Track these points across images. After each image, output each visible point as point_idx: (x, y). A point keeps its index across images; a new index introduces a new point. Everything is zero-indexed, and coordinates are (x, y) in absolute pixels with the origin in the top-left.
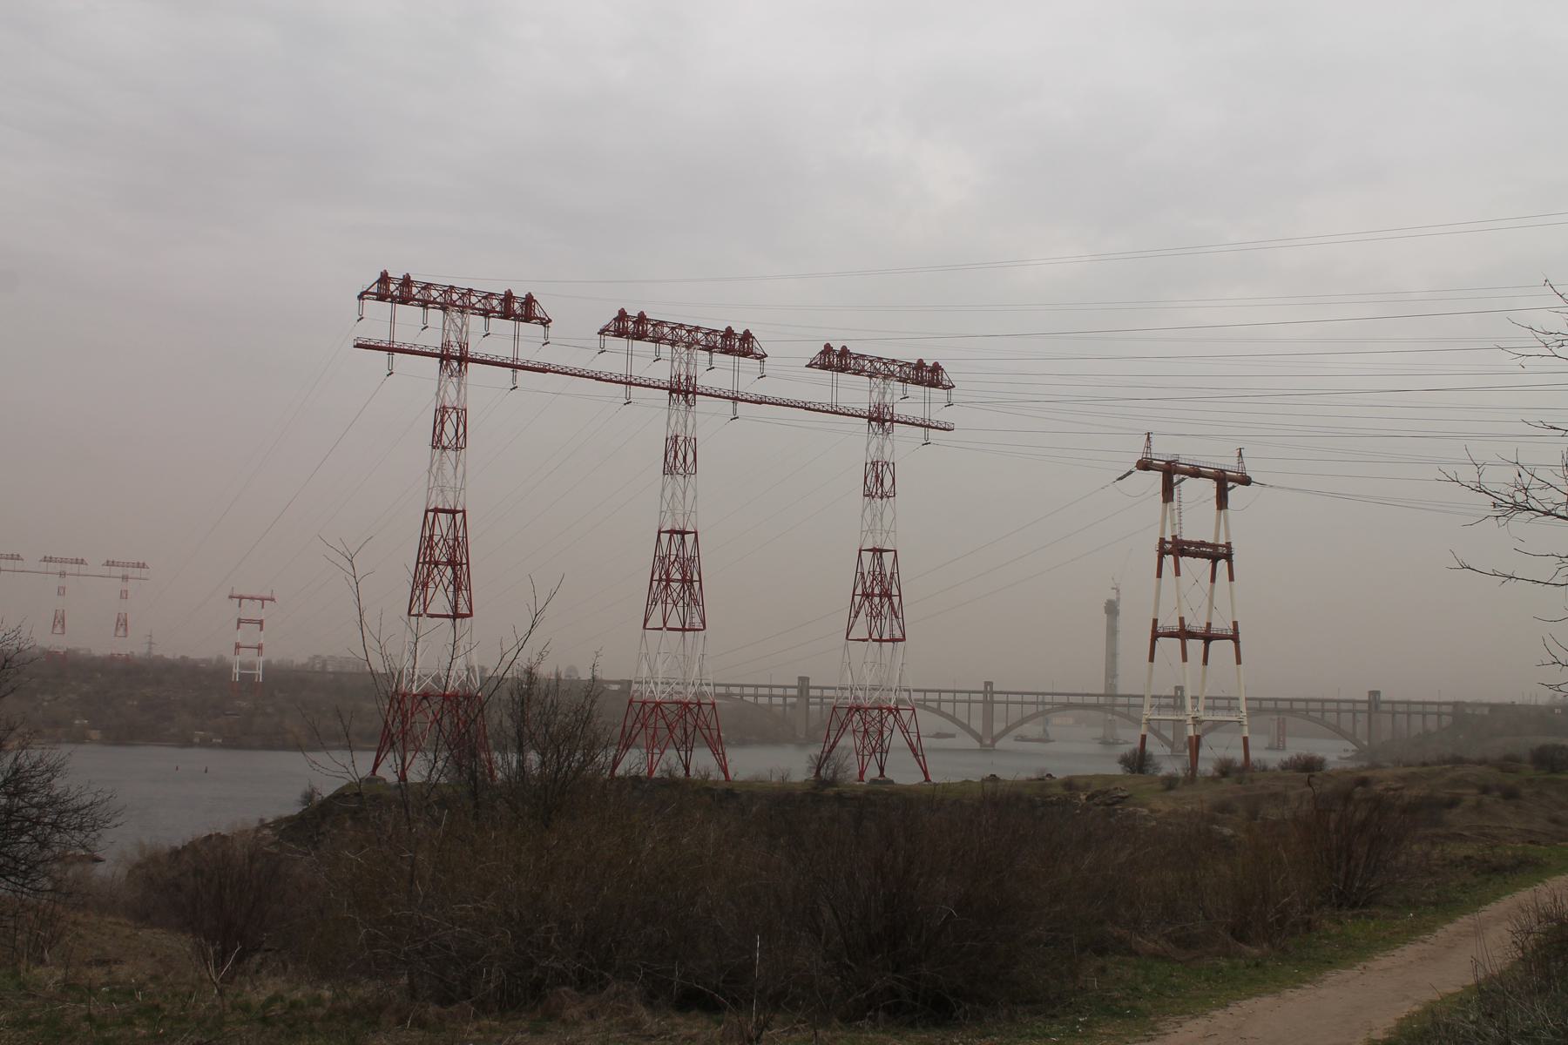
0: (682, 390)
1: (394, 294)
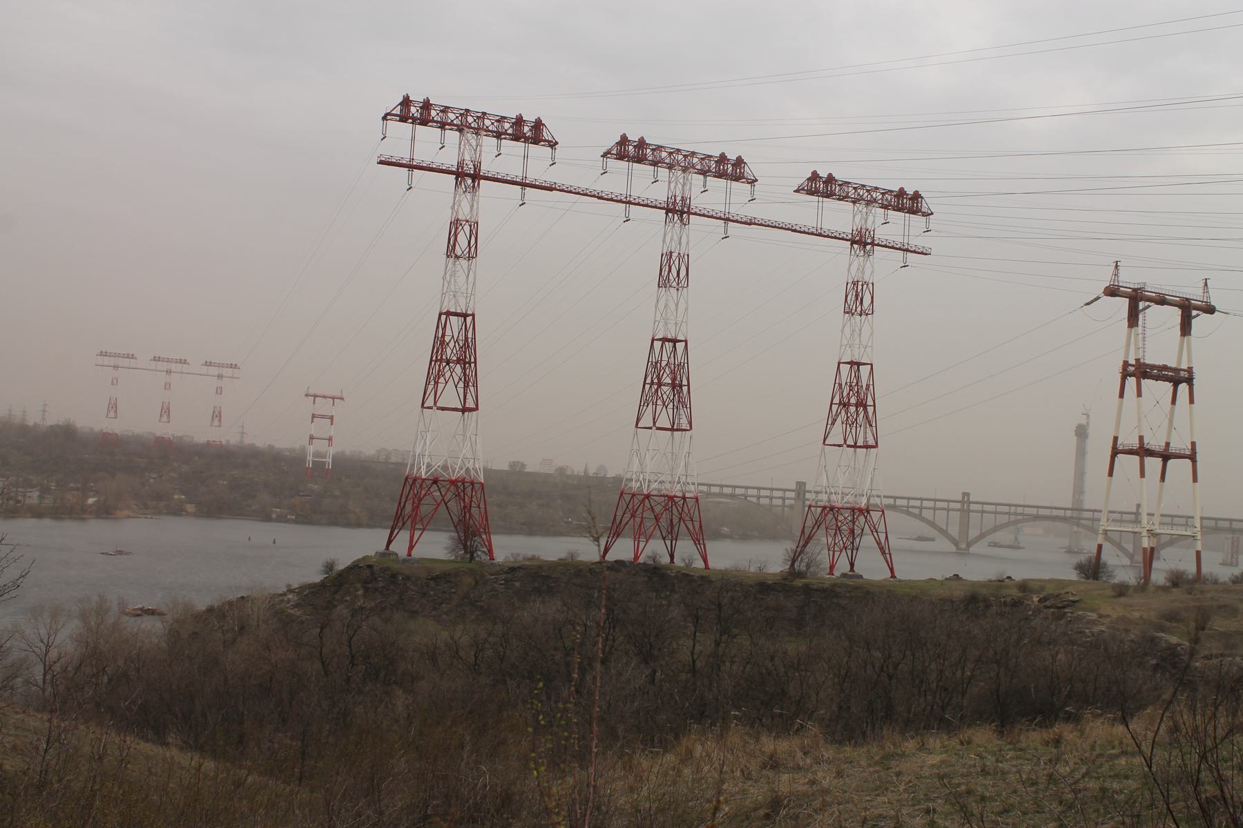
0: (678, 210)
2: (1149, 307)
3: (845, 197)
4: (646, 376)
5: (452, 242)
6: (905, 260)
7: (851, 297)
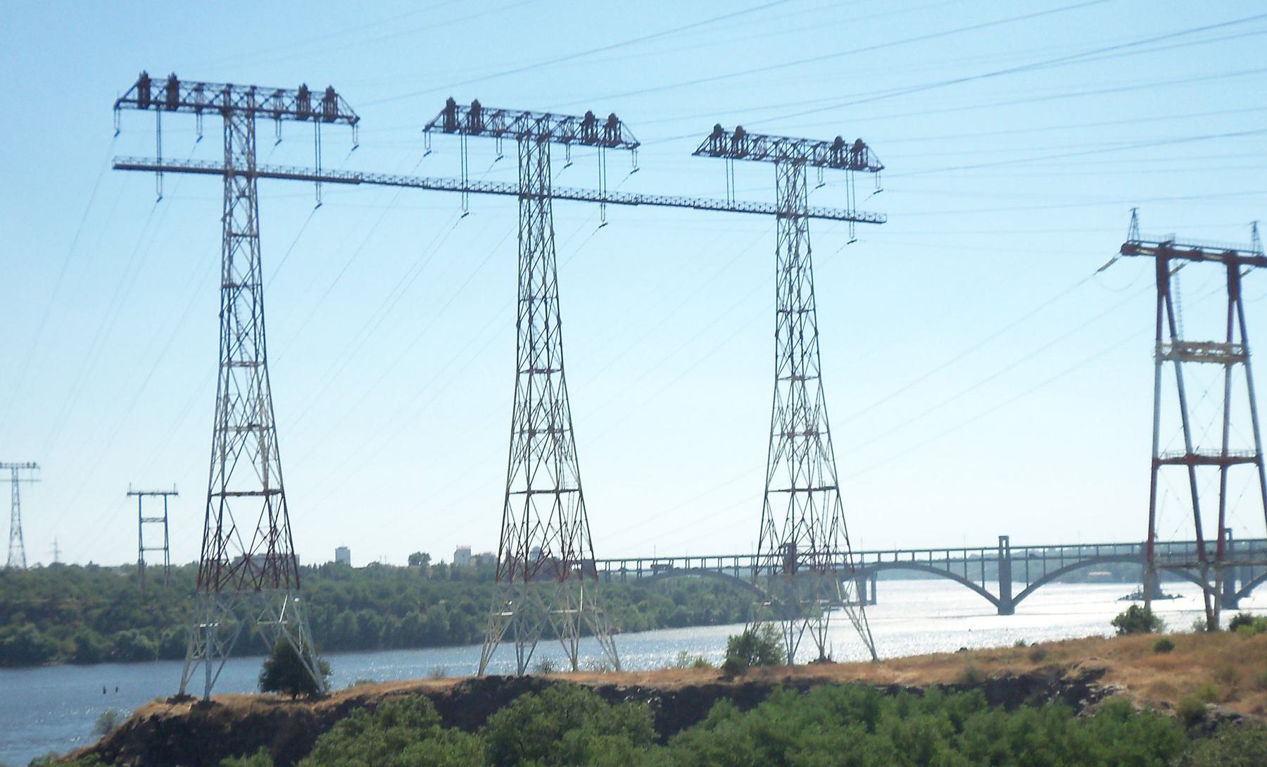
1: (317, 111)
2: (1182, 266)
3: (762, 157)
4: (513, 422)
5: (226, 267)
6: (852, 233)
7: (784, 290)
